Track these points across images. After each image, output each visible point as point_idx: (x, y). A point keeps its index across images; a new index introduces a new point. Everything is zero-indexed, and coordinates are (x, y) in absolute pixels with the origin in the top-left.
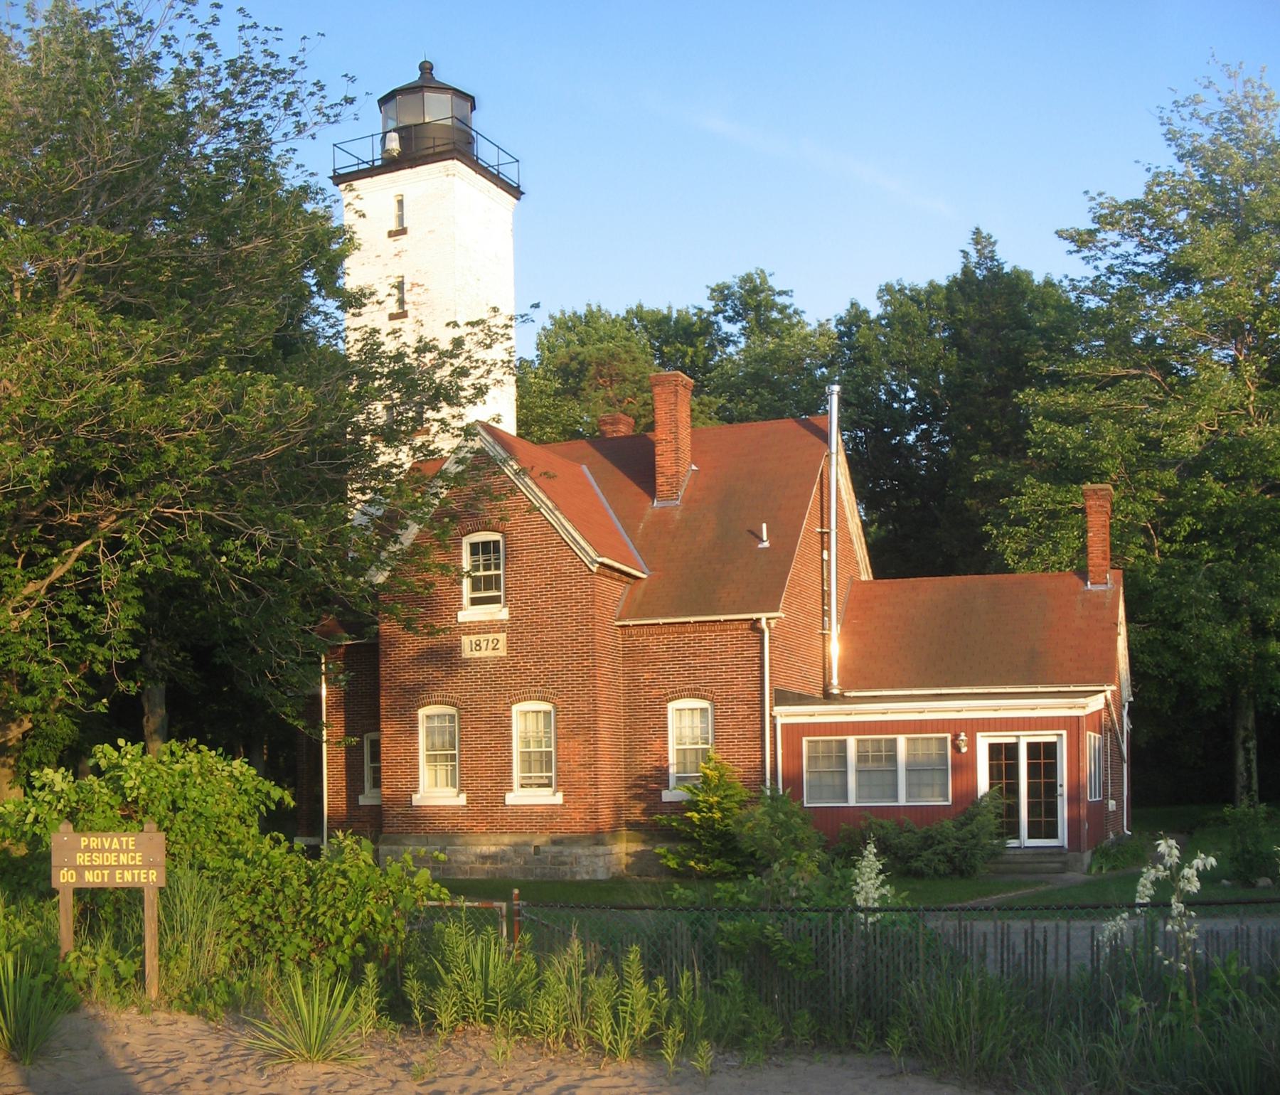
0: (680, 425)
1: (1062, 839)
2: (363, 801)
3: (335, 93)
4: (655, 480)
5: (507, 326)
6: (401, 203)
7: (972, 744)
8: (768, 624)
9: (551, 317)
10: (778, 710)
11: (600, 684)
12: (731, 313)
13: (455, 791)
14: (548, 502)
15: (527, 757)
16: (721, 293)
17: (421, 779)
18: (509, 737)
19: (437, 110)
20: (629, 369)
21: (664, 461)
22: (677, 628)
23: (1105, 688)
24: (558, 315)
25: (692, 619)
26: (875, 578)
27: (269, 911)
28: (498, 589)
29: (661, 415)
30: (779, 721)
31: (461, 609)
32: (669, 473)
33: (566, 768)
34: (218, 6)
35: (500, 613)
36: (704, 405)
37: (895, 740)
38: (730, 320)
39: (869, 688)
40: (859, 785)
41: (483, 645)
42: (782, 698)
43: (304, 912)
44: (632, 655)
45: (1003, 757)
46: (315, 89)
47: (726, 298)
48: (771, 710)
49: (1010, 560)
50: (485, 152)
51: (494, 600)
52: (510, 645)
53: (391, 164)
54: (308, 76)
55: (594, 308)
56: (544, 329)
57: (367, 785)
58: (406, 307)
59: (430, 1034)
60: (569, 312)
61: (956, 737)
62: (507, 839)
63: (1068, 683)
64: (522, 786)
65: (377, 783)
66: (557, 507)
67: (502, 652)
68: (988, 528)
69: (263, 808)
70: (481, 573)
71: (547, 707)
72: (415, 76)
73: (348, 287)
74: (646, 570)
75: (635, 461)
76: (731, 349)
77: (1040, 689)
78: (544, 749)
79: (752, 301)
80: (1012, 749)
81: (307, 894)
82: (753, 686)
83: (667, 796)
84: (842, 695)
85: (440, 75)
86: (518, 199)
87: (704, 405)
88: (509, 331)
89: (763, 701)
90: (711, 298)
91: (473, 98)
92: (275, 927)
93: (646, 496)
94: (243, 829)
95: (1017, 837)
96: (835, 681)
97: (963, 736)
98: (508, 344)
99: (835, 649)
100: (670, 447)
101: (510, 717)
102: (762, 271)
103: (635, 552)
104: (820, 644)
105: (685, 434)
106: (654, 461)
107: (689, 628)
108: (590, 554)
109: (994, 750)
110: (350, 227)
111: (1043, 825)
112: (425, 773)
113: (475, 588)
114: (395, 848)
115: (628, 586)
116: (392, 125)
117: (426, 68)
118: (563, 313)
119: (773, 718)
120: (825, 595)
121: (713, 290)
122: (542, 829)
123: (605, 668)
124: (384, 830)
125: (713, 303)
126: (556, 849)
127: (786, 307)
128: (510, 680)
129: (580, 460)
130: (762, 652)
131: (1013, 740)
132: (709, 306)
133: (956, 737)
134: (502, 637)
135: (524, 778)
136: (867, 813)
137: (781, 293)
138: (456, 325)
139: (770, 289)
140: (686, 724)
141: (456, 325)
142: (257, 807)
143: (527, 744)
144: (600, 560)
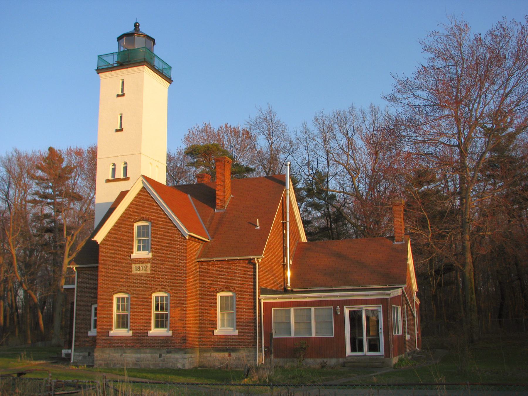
4: (215, 201)
8: (258, 261)
10: (262, 296)
11: (188, 285)
22: (222, 262)
23: (402, 286)
25: (227, 259)
30: (262, 301)
32: (221, 197)
37: (290, 309)
40: (316, 328)
42: (264, 291)
45: (355, 318)
48: (259, 296)
50: (157, 64)
52: (152, 268)
72: (131, 29)
74: (210, 237)
77: (374, 287)
82: (252, 286)
97: (338, 308)
103: (206, 231)
105: (228, 182)
107: (211, 263)
115: (202, 245)
117: (137, 26)
119: (260, 300)
120: (285, 249)
128: (149, 283)
144: (189, 234)
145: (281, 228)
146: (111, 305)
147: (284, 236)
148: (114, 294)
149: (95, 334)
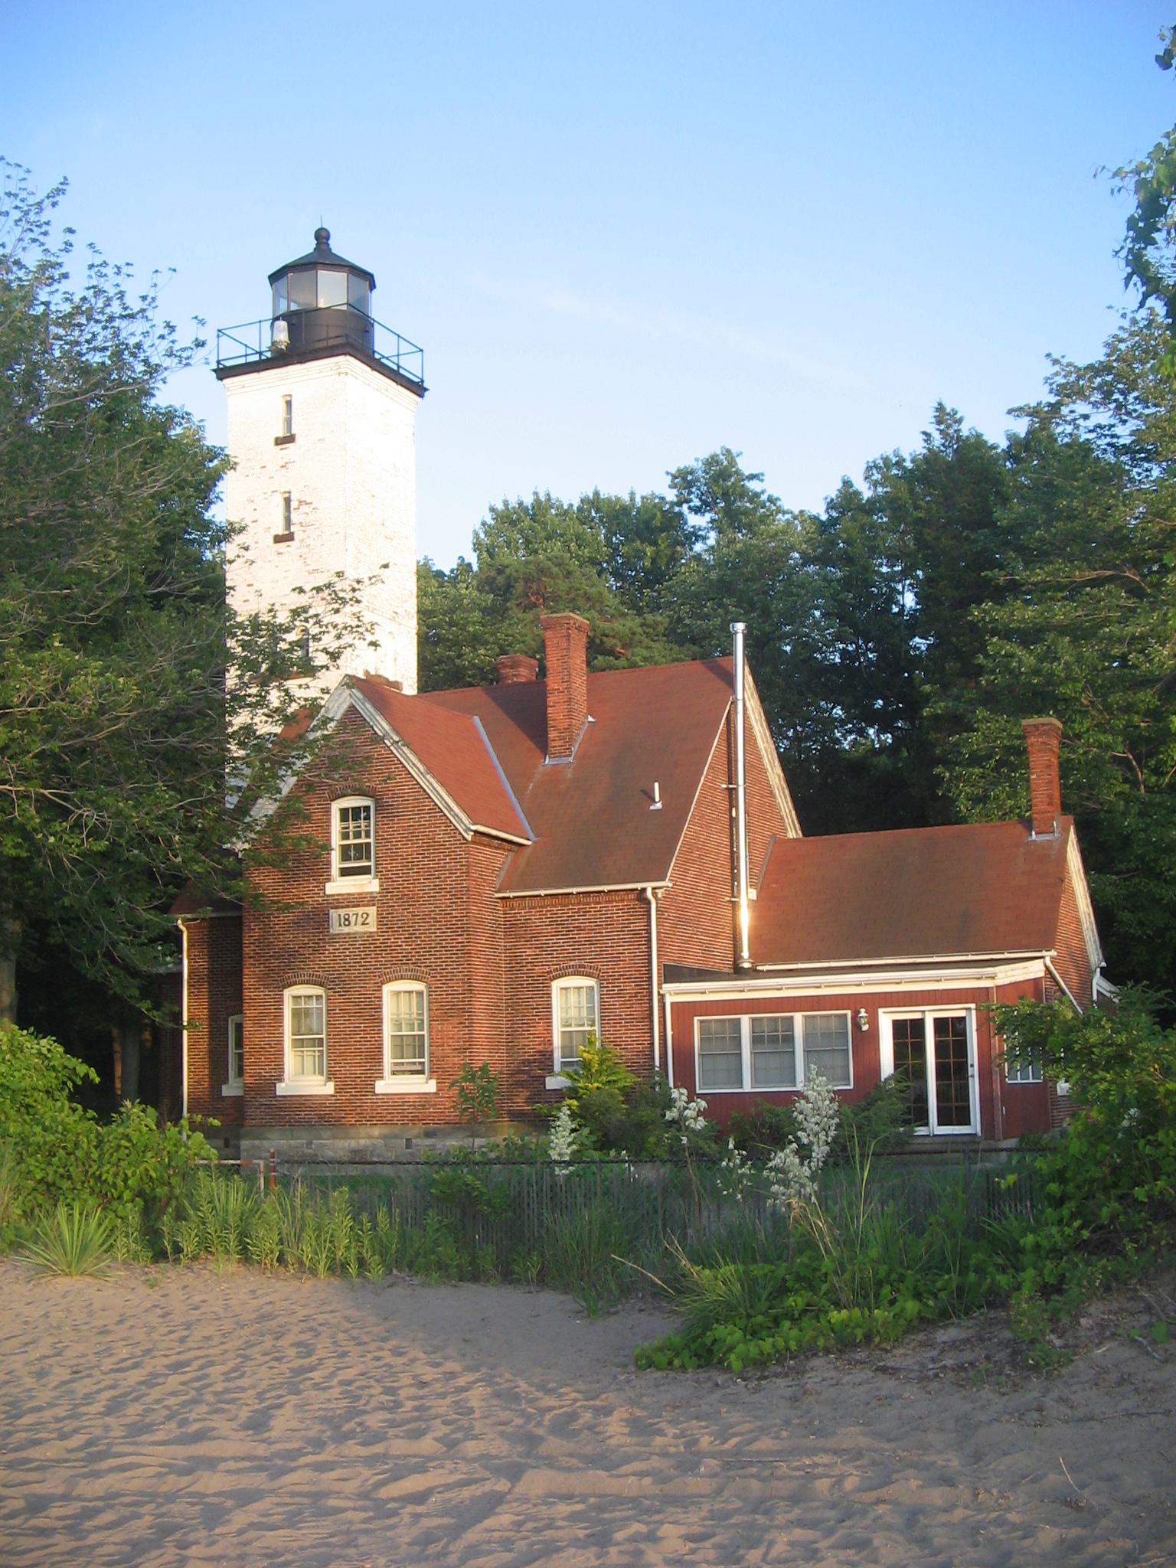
0: (574, 673)
1: (975, 1126)
2: (227, 1091)
3: (184, 338)
5: (354, 590)
6: (289, 403)
7: (874, 1021)
8: (654, 894)
9: (492, 510)
12: (697, 502)
13: (323, 1078)
14: (419, 765)
15: (399, 1042)
16: (683, 479)
17: (286, 1067)
18: (380, 1020)
19: (330, 292)
20: (563, 585)
21: (556, 712)
23: (1044, 953)
24: (500, 507)
25: (575, 890)
26: (804, 835)
27: (61, 1170)
28: (369, 858)
29: (553, 661)
30: (669, 1000)
31: (329, 880)
32: (562, 726)
33: (439, 1053)
34: (71, 231)
35: (370, 884)
36: (649, 626)
38: (697, 510)
39: (785, 961)
40: (755, 1069)
41: (353, 919)
42: (673, 974)
43: (91, 1171)
44: (515, 930)
45: (908, 1034)
46: (166, 331)
47: (689, 485)
48: (660, 987)
49: (962, 806)
50: (383, 344)
51: (365, 871)
53: (279, 358)
54: (158, 316)
55: (543, 498)
56: (484, 524)
57: (232, 1073)
58: (293, 529)
59: (177, 1261)
60: (513, 503)
61: (856, 1014)
62: (376, 1131)
63: (1001, 950)
64: (394, 1073)
65: (241, 1072)
66: (430, 770)
67: (372, 928)
68: (937, 770)
69: (70, 1084)
70: (352, 841)
71: (419, 986)
72: (307, 246)
73: (217, 520)
74: (531, 835)
75: (528, 714)
76: (698, 547)
78: (416, 1033)
79: (721, 485)
80: (918, 1025)
81: (95, 1155)
83: (552, 1083)
84: (755, 970)
85: (338, 246)
86: (421, 396)
87: (649, 626)
88: (357, 594)
89: (650, 978)
90: (673, 486)
91: (372, 276)
92: (66, 1185)
93: (539, 752)
94: (50, 1102)
95: (927, 1124)
96: (745, 954)
97: (863, 1013)
98: (356, 608)
99: (745, 919)
100: (562, 697)
101: (380, 998)
102: (728, 451)
103: (522, 815)
104: (729, 913)
106: (546, 713)
108: (465, 825)
109: (899, 1027)
110: (222, 449)
111: (954, 1110)
112: (290, 1059)
113: (345, 857)
114: (257, 1142)
115: (511, 854)
116: (283, 308)
117: (322, 236)
118: (506, 503)
119: (662, 997)
121: (675, 477)
122: (415, 1119)
123: (482, 944)
124: (248, 1122)
125: (675, 492)
126: (429, 1141)
127: (757, 495)
128: (381, 958)
129: (470, 711)
130: (649, 925)
131: (918, 1016)
132: (671, 495)
133: (856, 1014)
134: (372, 911)
135: (396, 1064)
136: (758, 1099)
137: (752, 477)
138: (301, 590)
139: (737, 473)
140: (571, 1004)
141: (301, 590)
142: (64, 1083)
143: (399, 1027)
144: (474, 828)
145: (725, 805)
146: (279, 1017)
147: (733, 822)
148: (285, 987)
149: (240, 1093)
